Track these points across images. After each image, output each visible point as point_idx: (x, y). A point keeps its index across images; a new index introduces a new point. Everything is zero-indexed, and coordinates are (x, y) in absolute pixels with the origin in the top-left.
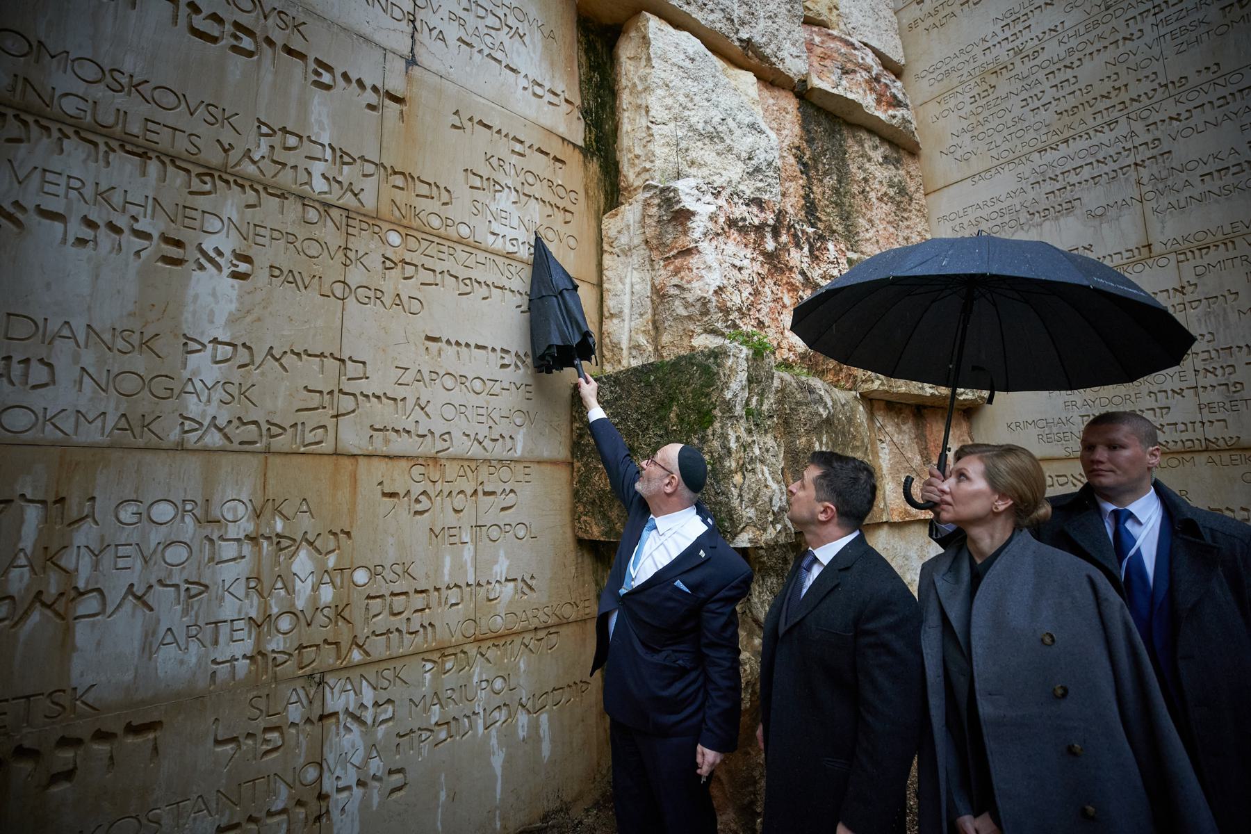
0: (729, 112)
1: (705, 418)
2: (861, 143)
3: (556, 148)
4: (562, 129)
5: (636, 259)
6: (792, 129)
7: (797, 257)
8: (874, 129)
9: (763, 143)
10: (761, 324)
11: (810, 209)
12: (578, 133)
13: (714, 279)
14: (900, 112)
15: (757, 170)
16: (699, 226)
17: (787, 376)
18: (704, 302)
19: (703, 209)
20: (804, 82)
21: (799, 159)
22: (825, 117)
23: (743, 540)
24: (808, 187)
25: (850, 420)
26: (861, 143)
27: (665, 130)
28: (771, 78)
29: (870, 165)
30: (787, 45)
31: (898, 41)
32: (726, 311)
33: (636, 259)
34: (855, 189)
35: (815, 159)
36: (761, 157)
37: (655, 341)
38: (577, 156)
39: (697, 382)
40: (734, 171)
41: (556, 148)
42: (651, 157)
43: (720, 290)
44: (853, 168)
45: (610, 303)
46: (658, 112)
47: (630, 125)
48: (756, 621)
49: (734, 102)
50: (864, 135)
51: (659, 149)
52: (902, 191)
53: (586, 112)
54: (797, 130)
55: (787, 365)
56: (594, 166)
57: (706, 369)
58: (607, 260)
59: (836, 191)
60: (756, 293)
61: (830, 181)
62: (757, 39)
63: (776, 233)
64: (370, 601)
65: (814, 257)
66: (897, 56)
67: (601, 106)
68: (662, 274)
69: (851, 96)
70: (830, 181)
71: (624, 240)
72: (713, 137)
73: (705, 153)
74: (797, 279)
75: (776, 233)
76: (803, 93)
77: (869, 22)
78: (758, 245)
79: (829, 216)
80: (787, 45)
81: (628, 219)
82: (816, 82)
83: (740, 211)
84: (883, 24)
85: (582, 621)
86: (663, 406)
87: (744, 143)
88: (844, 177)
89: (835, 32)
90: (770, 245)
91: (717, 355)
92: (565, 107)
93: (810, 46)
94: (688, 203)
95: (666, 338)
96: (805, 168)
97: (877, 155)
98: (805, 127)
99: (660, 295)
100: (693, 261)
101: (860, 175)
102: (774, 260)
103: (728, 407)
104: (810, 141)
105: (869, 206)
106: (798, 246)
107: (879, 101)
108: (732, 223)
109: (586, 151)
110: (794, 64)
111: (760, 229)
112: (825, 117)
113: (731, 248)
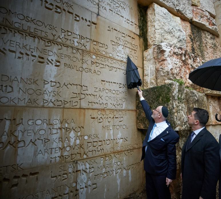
1: (168, 100)
2: (205, 34)
3: (132, 35)
4: (134, 31)
5: (152, 62)
6: (189, 31)
7: (190, 61)
9: (182, 34)
10: (181, 77)
11: (193, 50)
12: (138, 32)
13: (170, 67)
14: (214, 27)
15: (181, 40)
16: (167, 54)
17: (188, 90)
18: (168, 72)
19: (168, 50)
20: (192, 20)
21: (190, 38)
23: (177, 129)
24: (193, 45)
25: (203, 100)
26: (205, 34)
28: (184, 19)
30: (188, 11)
31: (214, 10)
32: (173, 74)
33: (152, 62)
34: (204, 45)
35: (194, 38)
36: (181, 37)
37: (156, 81)
38: (138, 37)
39: (166, 91)
40: (175, 41)
41: (132, 35)
42: (155, 37)
43: (171, 69)
44: (203, 40)
45: (146, 72)
46: (157, 27)
47: (150, 30)
49: (175, 24)
50: (206, 32)
51: (157, 36)
52: (215, 46)
53: (140, 27)
54: (190, 31)
55: (187, 87)
56: (142, 40)
57: (168, 88)
58: (145, 62)
59: (199, 46)
60: (180, 70)
61: (198, 43)
62: (181, 9)
63: (185, 56)
65: (194, 61)
67: (143, 25)
68: (158, 65)
69: (203, 23)
70: (198, 43)
71: (149, 57)
72: (170, 33)
73: (168, 36)
74: (190, 67)
75: (185, 56)
78: (181, 58)
79: (198, 51)
80: (188, 11)
83: (176, 50)
86: (158, 97)
87: (177, 34)
88: (201, 42)
90: (184, 58)
91: (171, 85)
93: (193, 11)
94: (164, 48)
97: (209, 37)
98: (192, 30)
99: (157, 70)
100: (165, 62)
101: (205, 42)
102: (185, 62)
103: (174, 97)
104: (193, 34)
105: (207, 49)
106: (190, 59)
107: (209, 24)
108: (174, 53)
109: (140, 36)
110: (189, 15)
111: (181, 55)
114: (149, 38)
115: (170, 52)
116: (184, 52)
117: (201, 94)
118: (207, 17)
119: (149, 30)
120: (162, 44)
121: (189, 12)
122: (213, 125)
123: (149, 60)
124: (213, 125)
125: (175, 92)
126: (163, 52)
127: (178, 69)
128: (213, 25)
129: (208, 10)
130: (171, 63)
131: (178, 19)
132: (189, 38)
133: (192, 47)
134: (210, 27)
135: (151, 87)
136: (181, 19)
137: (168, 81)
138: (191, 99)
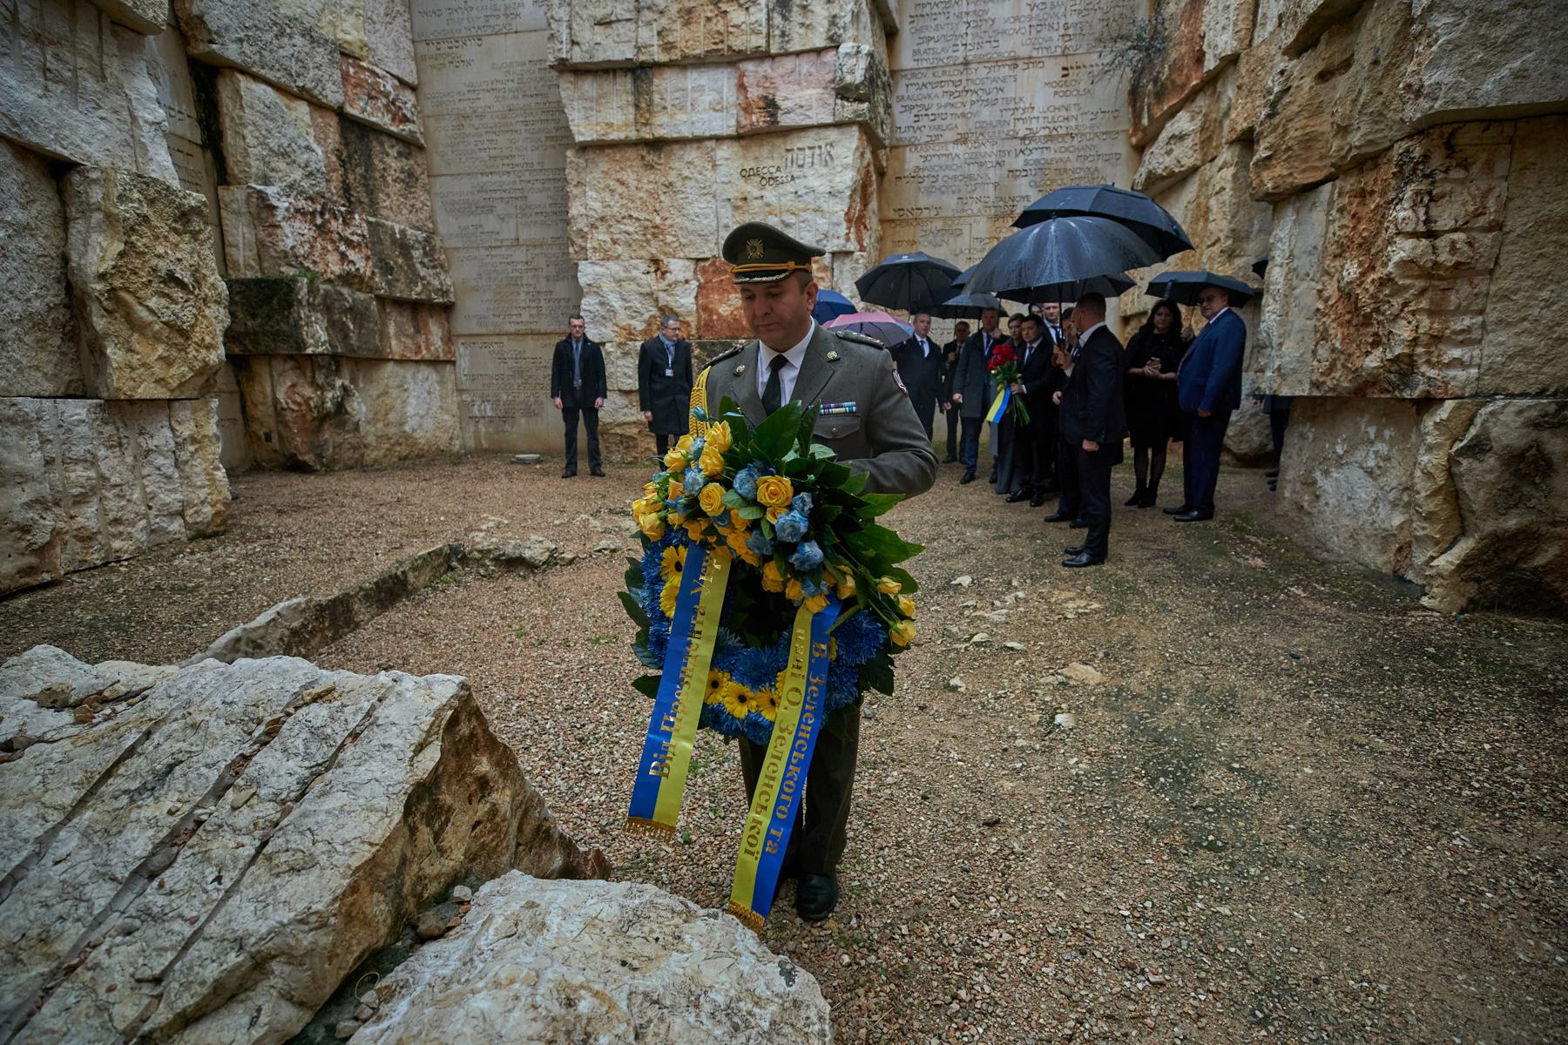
0: (293, 140)
1: (290, 305)
2: (382, 144)
3: (186, 148)
4: (188, 135)
6: (334, 138)
7: (335, 225)
8: (390, 135)
10: (315, 263)
11: (346, 189)
12: (197, 136)
13: (290, 242)
14: (410, 126)
15: (311, 174)
16: (280, 214)
17: (328, 287)
18: (286, 253)
19: (283, 204)
21: (339, 158)
22: (356, 133)
23: (309, 351)
24: (345, 175)
25: (367, 309)
26: (382, 144)
27: (256, 151)
28: (317, 105)
29: (391, 162)
30: (329, 85)
31: (413, 66)
32: (297, 257)
34: (377, 175)
35: (350, 157)
37: (260, 264)
38: (199, 151)
39: (285, 290)
40: (297, 175)
42: (249, 166)
43: (293, 248)
44: (376, 162)
45: (229, 239)
46: (250, 140)
48: (149, 99)
50: (384, 138)
52: (411, 174)
53: (200, 121)
54: (337, 138)
55: (329, 281)
56: (209, 155)
57: (289, 286)
58: (224, 214)
59: (364, 177)
60: (312, 247)
61: (360, 171)
62: (309, 85)
63: (322, 214)
64: (567, 89)
65: (345, 223)
66: (411, 79)
68: (262, 234)
69: (373, 119)
70: (360, 171)
71: (235, 206)
72: (285, 154)
73: (281, 164)
74: (336, 237)
75: (322, 214)
76: (340, 113)
77: (391, 54)
78: (312, 222)
79: (359, 193)
80: (329, 85)
81: (235, 196)
82: (349, 110)
83: (302, 203)
84: (402, 54)
85: (231, 393)
88: (369, 166)
89: (364, 64)
90: (319, 221)
91: (294, 280)
92: (188, 121)
93: (345, 77)
94: (274, 202)
95: (266, 265)
96: (343, 163)
97: (393, 152)
99: (261, 245)
100: (279, 231)
102: (322, 230)
103: (300, 302)
104: (347, 145)
105: (387, 185)
106: (336, 219)
107: (393, 119)
108: (297, 211)
109: (203, 147)
110: (333, 94)
111: (313, 213)
112: (356, 131)
113: (297, 224)
114: (231, 161)
115: (287, 210)
116: (319, 207)
117: (361, 296)
118: (387, 95)
119: (229, 137)
120: (270, 190)
121: (334, 88)
122: (396, 361)
123: (237, 213)
124: (396, 361)
125: (303, 293)
126: (273, 208)
127: (307, 246)
128: (405, 120)
129: (395, 72)
130: (288, 230)
131: (303, 108)
132: (334, 159)
133: (344, 182)
134: (394, 129)
135: (250, 275)
136: (310, 103)
137: (291, 272)
138: (337, 305)
